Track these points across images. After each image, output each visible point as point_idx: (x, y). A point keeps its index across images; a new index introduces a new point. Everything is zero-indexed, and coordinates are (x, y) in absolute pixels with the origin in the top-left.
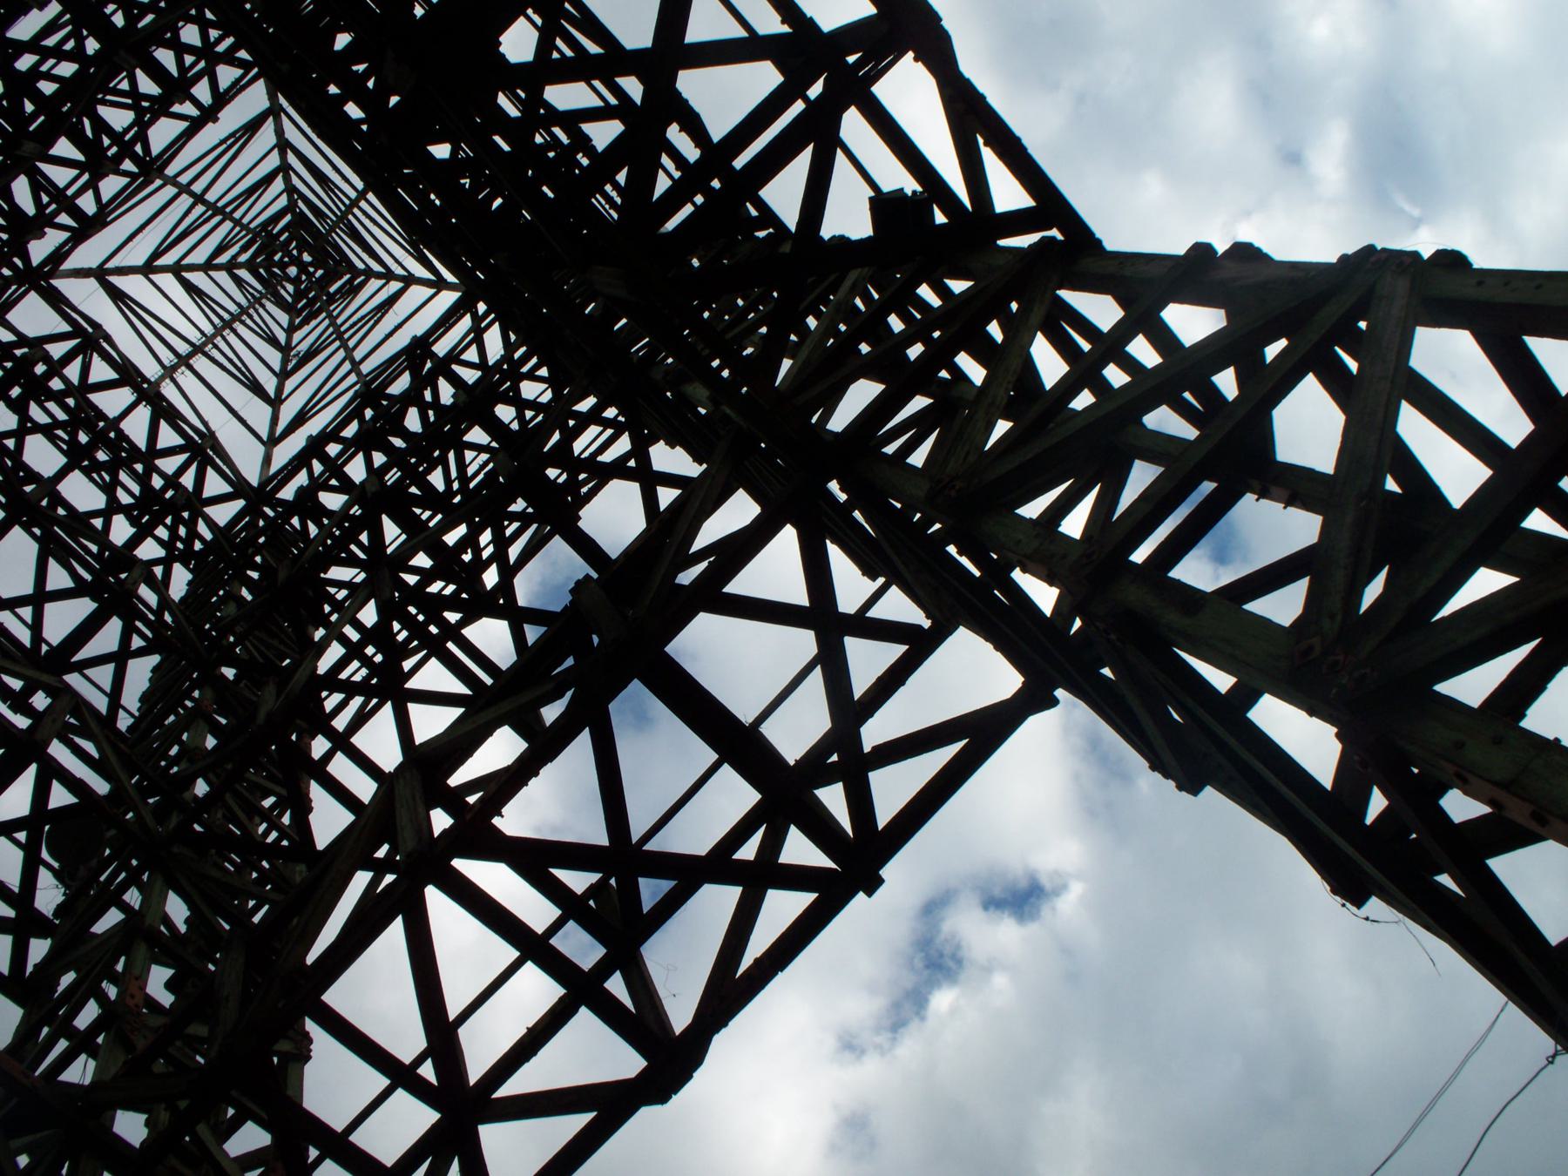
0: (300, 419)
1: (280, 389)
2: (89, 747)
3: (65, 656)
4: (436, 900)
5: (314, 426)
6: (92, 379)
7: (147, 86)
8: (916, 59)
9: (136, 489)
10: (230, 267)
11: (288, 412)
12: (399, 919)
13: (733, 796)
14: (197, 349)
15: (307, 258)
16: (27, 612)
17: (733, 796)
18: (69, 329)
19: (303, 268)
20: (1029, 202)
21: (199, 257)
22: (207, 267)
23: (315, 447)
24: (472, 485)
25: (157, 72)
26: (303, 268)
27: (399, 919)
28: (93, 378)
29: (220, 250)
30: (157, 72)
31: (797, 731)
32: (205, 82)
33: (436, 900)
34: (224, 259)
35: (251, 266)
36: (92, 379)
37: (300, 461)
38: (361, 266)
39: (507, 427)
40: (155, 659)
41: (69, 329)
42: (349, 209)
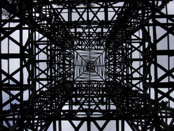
0: (98, 53)
1: (81, 74)
2: (31, 92)
3: (39, 80)
4: (85, 123)
5: (83, 80)
6: (164, 73)
7: (111, 63)
8: (100, 32)
9: (60, 69)
10: (85, 62)
11: (81, 77)
12: (80, 121)
13: (109, 9)
14: (101, 66)
15: (89, 66)
16: (40, 72)
17: (109, 9)
18: (19, 42)
19: (90, 66)
20: (137, 86)
21: (84, 59)
22: (84, 60)
23: (97, 49)
24: (91, 116)
25: (112, 65)
26: (90, 66)
27: (80, 121)
28: (164, 73)
29: (86, 60)
30: (112, 65)
31: (102, 10)
32: (84, 46)
33: (85, 123)
34: (86, 61)
35: (87, 63)
36: (164, 73)
37: (100, 49)
38: (95, 71)
39: (103, 100)
40: (47, 90)
41: (19, 42)
42: (80, 66)
